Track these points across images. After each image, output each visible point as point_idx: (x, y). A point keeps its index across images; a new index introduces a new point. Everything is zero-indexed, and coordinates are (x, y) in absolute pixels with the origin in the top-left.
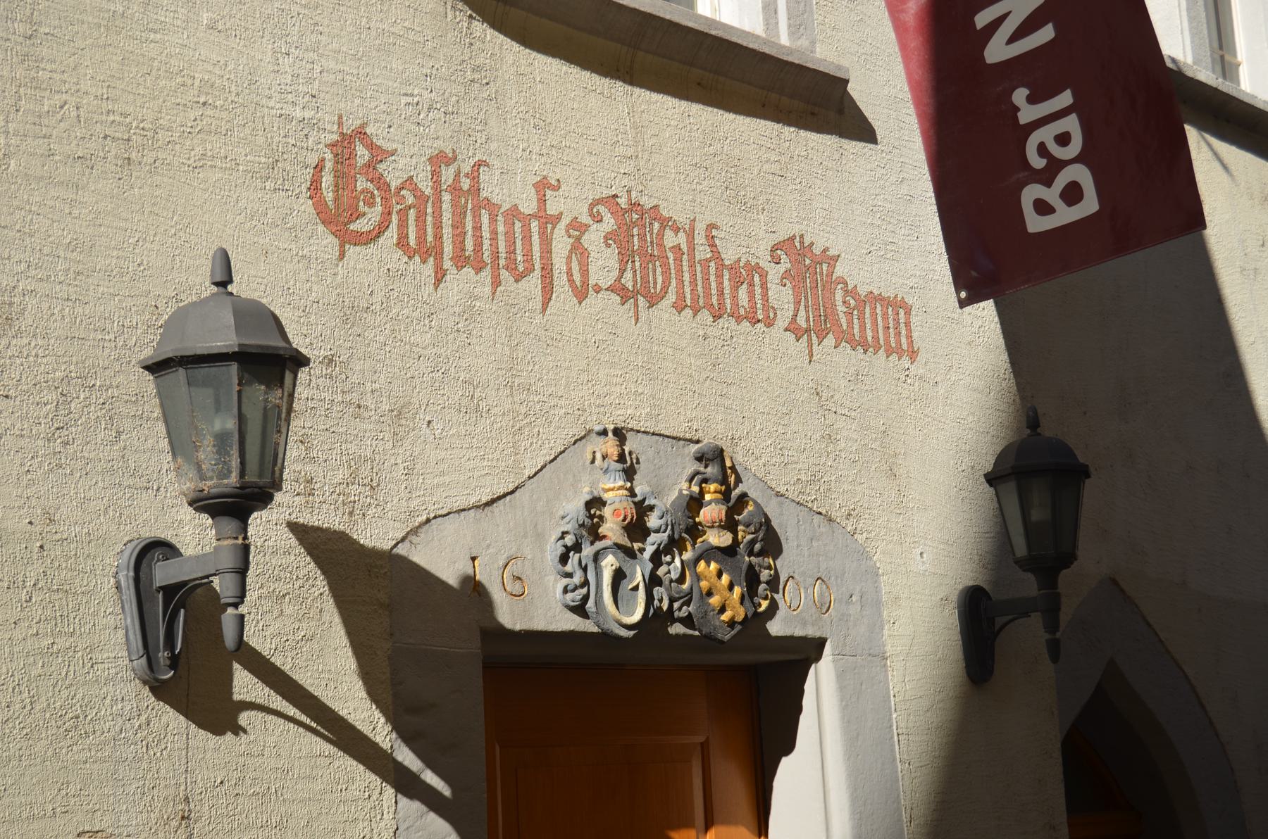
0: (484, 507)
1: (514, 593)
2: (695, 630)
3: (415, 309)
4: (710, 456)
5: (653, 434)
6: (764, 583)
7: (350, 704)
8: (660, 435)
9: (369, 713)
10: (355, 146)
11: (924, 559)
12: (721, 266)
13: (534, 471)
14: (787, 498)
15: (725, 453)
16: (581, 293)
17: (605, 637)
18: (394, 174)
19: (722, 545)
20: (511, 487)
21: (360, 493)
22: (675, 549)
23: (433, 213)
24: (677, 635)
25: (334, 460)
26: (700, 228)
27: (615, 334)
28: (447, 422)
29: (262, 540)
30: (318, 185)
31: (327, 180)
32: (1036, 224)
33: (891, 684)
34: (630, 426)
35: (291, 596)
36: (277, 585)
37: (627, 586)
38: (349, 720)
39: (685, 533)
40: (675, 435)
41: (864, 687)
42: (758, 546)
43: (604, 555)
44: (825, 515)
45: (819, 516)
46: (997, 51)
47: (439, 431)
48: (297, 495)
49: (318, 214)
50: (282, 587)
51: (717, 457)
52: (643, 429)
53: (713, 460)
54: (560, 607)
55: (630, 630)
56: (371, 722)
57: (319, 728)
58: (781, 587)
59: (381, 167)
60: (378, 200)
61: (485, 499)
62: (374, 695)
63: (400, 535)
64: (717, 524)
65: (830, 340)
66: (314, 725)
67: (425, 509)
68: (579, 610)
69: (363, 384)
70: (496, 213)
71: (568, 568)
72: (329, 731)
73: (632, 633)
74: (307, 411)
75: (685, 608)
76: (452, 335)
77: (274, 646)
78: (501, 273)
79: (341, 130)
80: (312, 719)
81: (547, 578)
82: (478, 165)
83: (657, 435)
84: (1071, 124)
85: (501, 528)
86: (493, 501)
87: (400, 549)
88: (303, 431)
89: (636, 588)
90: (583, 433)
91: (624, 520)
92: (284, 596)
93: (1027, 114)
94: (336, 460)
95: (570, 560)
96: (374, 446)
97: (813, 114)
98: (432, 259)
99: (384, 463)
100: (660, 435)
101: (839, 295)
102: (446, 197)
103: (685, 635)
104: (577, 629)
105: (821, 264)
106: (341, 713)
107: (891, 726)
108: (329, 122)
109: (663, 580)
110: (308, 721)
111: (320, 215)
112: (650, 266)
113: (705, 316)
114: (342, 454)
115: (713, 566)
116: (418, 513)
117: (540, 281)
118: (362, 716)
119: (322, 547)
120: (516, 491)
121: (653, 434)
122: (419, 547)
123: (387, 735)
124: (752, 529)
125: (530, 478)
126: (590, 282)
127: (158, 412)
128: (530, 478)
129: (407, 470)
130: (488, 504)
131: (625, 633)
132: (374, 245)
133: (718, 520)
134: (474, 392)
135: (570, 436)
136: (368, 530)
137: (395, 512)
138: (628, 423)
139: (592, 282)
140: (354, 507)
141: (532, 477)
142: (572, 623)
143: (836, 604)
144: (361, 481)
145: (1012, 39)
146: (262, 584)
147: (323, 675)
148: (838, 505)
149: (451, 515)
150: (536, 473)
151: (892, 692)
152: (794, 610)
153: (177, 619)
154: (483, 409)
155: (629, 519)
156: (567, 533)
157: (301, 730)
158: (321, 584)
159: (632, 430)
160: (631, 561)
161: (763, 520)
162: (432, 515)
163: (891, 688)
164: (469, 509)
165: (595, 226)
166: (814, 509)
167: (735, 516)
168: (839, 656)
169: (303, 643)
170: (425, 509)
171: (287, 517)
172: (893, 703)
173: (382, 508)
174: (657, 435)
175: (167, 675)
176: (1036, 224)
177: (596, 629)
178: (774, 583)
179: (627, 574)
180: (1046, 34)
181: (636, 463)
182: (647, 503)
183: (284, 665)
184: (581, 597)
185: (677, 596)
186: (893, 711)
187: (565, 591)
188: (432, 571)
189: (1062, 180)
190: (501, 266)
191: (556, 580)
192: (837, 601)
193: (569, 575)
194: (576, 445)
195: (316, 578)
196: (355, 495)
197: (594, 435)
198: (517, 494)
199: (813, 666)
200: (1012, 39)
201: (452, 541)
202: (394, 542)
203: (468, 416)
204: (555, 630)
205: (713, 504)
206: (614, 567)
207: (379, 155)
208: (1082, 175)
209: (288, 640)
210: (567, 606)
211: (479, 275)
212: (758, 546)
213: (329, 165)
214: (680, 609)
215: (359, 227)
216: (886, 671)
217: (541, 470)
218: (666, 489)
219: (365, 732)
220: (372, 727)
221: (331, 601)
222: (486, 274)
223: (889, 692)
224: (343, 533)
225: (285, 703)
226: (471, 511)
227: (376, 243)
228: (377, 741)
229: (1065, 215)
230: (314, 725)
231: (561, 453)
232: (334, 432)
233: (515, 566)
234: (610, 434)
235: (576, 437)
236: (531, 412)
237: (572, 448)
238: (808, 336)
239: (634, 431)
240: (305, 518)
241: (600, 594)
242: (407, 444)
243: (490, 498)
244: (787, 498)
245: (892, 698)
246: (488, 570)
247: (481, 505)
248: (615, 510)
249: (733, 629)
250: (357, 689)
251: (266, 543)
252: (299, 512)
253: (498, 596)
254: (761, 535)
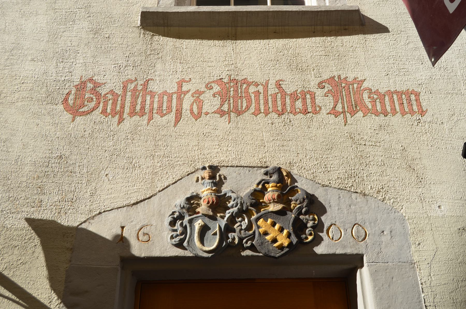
0: (132, 205)
1: (143, 241)
2: (259, 253)
3: (106, 134)
4: (271, 172)
5: (237, 166)
6: (310, 227)
7: (40, 291)
8: (241, 167)
9: (49, 295)
10: (87, 84)
11: (442, 209)
12: (284, 94)
13: (162, 188)
14: (330, 187)
15: (282, 170)
16: (197, 116)
17: (197, 258)
18: (103, 91)
19: (274, 210)
20: (148, 196)
21: (65, 204)
22: (244, 215)
23: (121, 100)
24: (247, 256)
25: (54, 193)
26: (272, 83)
27: (216, 129)
28: (116, 173)
29: (11, 225)
30: (67, 99)
31: (71, 97)
33: (419, 278)
34: (222, 165)
35: (19, 247)
36: (13, 243)
37: (209, 234)
38: (38, 298)
39: (251, 206)
40: (251, 165)
41: (394, 279)
42: (304, 210)
43: (196, 221)
44: (360, 193)
45: (356, 194)
47: (112, 177)
48: (32, 207)
49: (65, 109)
50: (15, 243)
51: (275, 172)
52: (230, 165)
53: (273, 173)
54: (170, 244)
55: (210, 253)
56: (49, 299)
57: (20, 301)
58: (325, 229)
59: (98, 89)
60: (95, 100)
61: (132, 202)
62: (54, 287)
63: (83, 220)
64: (272, 201)
65: (360, 114)
66: (18, 300)
67: (99, 209)
68: (180, 245)
69: (75, 164)
70: (154, 95)
71: (176, 228)
72: (25, 303)
73: (210, 255)
74: (44, 176)
75: (249, 242)
76: (124, 141)
77: (5, 267)
78: (154, 115)
79: (81, 80)
80: (17, 297)
81: (164, 233)
82: (152, 79)
83: (239, 167)
85: (140, 214)
86: (137, 203)
87: (83, 226)
88: (41, 184)
89: (215, 234)
90: (194, 170)
91: (208, 203)
92: (16, 247)
94: (55, 193)
95: (177, 224)
96: (76, 186)
97: (345, 29)
98: (118, 115)
99: (80, 192)
100: (241, 167)
101: (365, 95)
102: (129, 94)
103: (252, 256)
104: (179, 255)
105: (353, 84)
106: (34, 295)
107: (420, 302)
108: (76, 79)
109: (236, 230)
110: (13, 297)
111: (66, 109)
112: (239, 101)
113: (274, 115)
114: (59, 190)
115: (269, 221)
116: (95, 210)
117: (174, 115)
118: (45, 296)
119: (40, 227)
120: (151, 197)
121: (237, 166)
122: (93, 224)
123: (57, 305)
124: (298, 202)
125: (159, 191)
126: (203, 112)
128: (159, 191)
129: (92, 194)
130: (134, 204)
131: (206, 255)
132: (90, 115)
133: (271, 199)
134: (133, 161)
135: (185, 172)
136: (67, 219)
137: (83, 211)
138: (221, 164)
139: (204, 111)
140: (61, 210)
141: (161, 191)
142: (178, 252)
143: (370, 236)
144: (67, 200)
146: (6, 242)
147: (28, 279)
148: (370, 188)
149: (113, 210)
150: (163, 190)
151: (420, 282)
152: (336, 241)
154: (136, 167)
155: (211, 202)
156: (175, 212)
157: (10, 302)
158: (37, 241)
159: (223, 166)
160: (214, 222)
161: (305, 197)
162: (102, 211)
163: (419, 279)
164: (123, 207)
165: (208, 91)
166: (352, 191)
167: (290, 198)
168: (373, 264)
169: (21, 265)
170: (99, 209)
171: (26, 216)
172: (421, 288)
173: (76, 209)
174: (239, 167)
177: (191, 255)
178: (318, 227)
179: (211, 228)
181: (224, 179)
182: (227, 195)
183: (8, 275)
184: (179, 239)
185: (244, 236)
186: (422, 293)
187: (172, 237)
188: (98, 234)
190: (154, 113)
191: (168, 233)
192: (370, 235)
193: (176, 231)
194: (189, 176)
195: (35, 239)
196: (62, 206)
197: (200, 170)
198: (152, 199)
199: (359, 270)
201: (111, 221)
202: (80, 223)
203: (128, 170)
204: (166, 256)
205: (270, 192)
206: (200, 225)
207: (97, 85)
209: (13, 264)
210: (173, 245)
211: (142, 118)
212: (304, 210)
213: (73, 92)
214: (246, 242)
215: (83, 110)
216: (415, 270)
217: (167, 187)
218: (243, 189)
219: (45, 303)
220: (49, 301)
221: (41, 248)
222: (146, 117)
223: (418, 282)
224: (53, 221)
225: (5, 291)
226: (124, 208)
227: (91, 114)
228: (51, 307)
230: (18, 300)
231: (179, 180)
232: (56, 183)
233: (145, 229)
234: (207, 168)
235: (189, 172)
236: (164, 165)
237: (187, 177)
238: (344, 114)
239: (225, 166)
240: (37, 216)
241: (192, 238)
242: (94, 184)
243: (135, 202)
244: (330, 187)
245: (420, 286)
246: (130, 231)
247: (130, 205)
248: (204, 200)
249: (283, 251)
250: (46, 284)
251: (12, 227)
252: (32, 214)
253: (133, 242)
254: (305, 204)
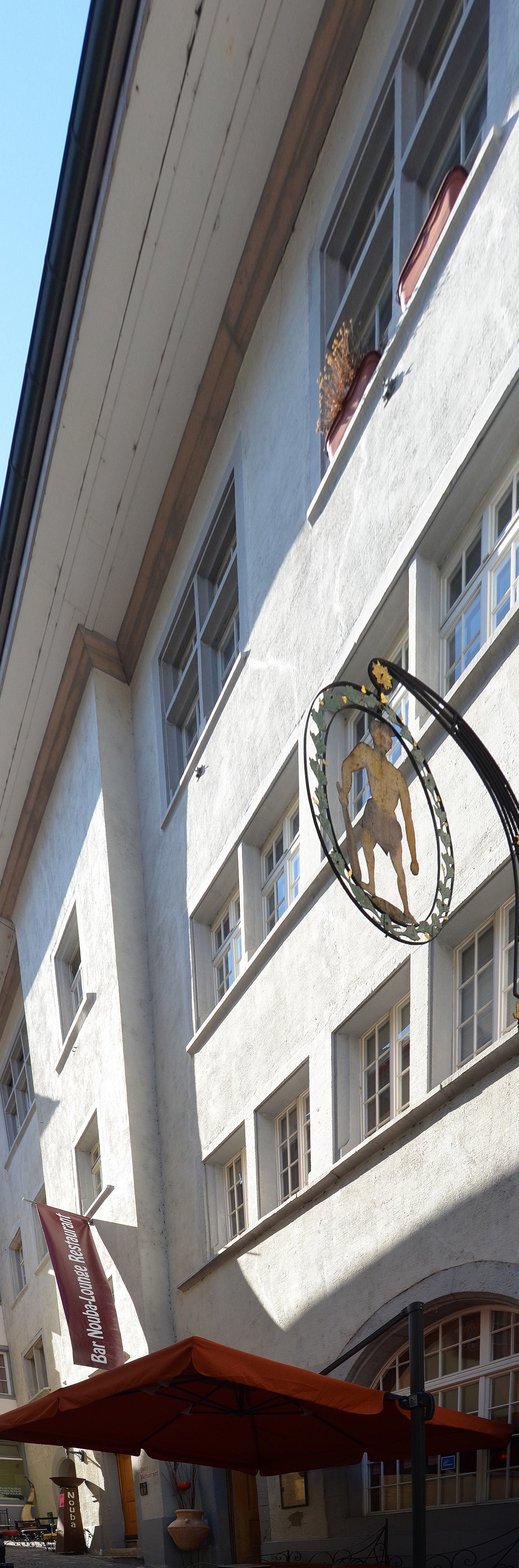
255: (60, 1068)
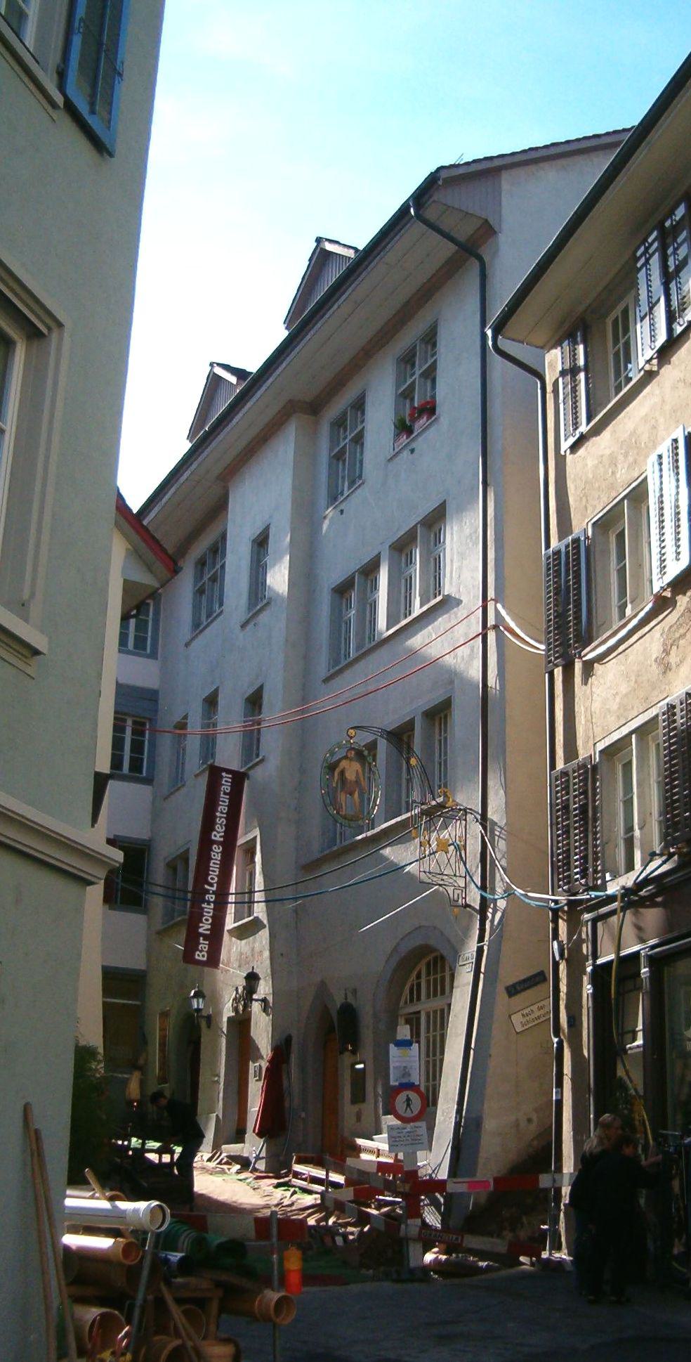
32: (197, 957)
46: (201, 930)
84: (207, 946)
93: (201, 941)
127: (442, 237)
145: (204, 930)
153: (647, 1022)
175: (121, 1320)
176: (197, 957)
180: (208, 932)
189: (203, 953)
200: (204, 930)
208: (206, 954)
229: (201, 958)
255: (243, 626)
